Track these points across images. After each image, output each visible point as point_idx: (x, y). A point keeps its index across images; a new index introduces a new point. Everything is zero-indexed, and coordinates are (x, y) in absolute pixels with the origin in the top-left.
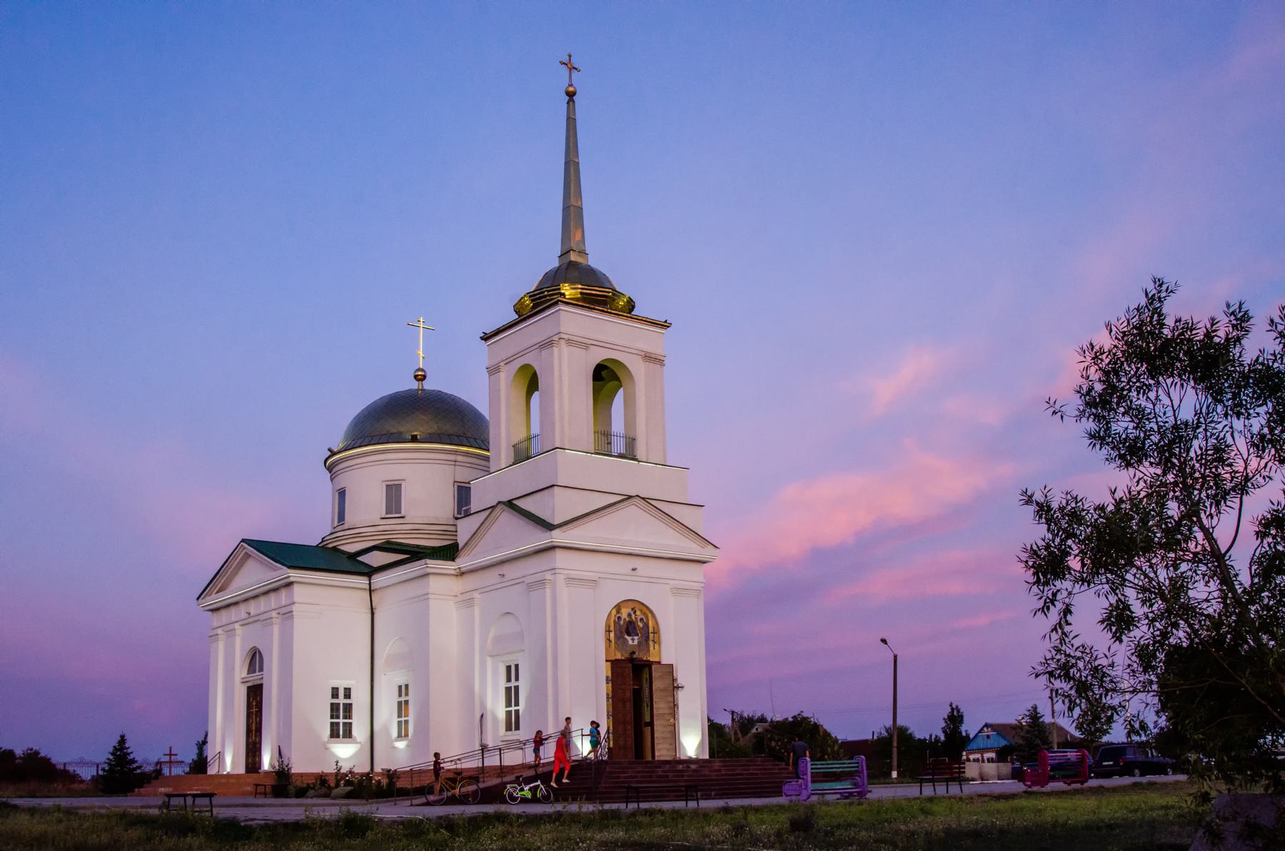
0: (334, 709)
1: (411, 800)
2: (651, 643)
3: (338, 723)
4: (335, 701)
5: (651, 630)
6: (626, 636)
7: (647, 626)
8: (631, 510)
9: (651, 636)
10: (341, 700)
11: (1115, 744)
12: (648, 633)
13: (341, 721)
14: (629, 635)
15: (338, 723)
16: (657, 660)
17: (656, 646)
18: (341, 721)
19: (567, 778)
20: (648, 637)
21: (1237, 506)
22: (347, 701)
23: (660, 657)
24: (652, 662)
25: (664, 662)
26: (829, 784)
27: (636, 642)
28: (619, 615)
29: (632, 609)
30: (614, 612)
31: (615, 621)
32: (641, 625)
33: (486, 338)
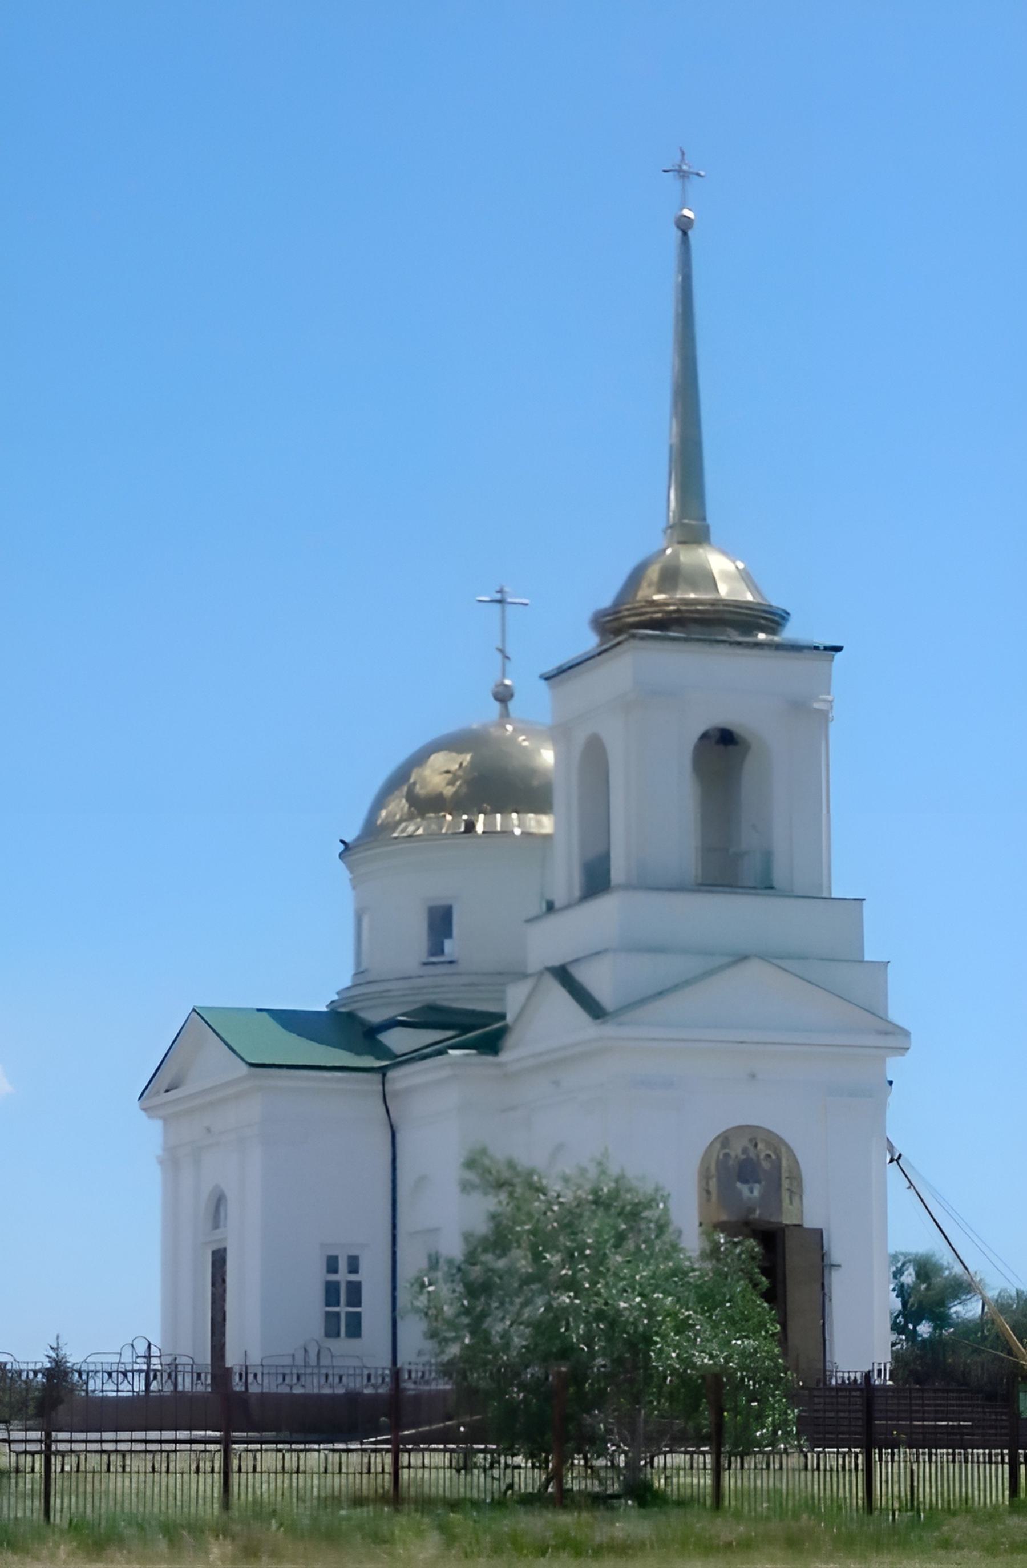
0: (331, 1293)
1: (232, 1472)
2: (785, 1195)
3: (338, 1314)
4: (333, 1277)
5: (784, 1174)
6: (739, 1185)
7: (777, 1166)
8: (754, 969)
9: (785, 1184)
10: (343, 1276)
11: (864, 1496)
12: (780, 1179)
13: (343, 1309)
14: (745, 1181)
15: (338, 1314)
16: (795, 1222)
17: (796, 1199)
18: (343, 1309)
19: (890, 1380)
20: (780, 1185)
21: (101, 1376)
22: (353, 1277)
23: (802, 1218)
24: (787, 1225)
25: (808, 1224)
26: (861, 1477)
27: (756, 1193)
28: (727, 1151)
29: (750, 1140)
30: (718, 1145)
31: (718, 1161)
32: (766, 1165)
33: (547, 678)
